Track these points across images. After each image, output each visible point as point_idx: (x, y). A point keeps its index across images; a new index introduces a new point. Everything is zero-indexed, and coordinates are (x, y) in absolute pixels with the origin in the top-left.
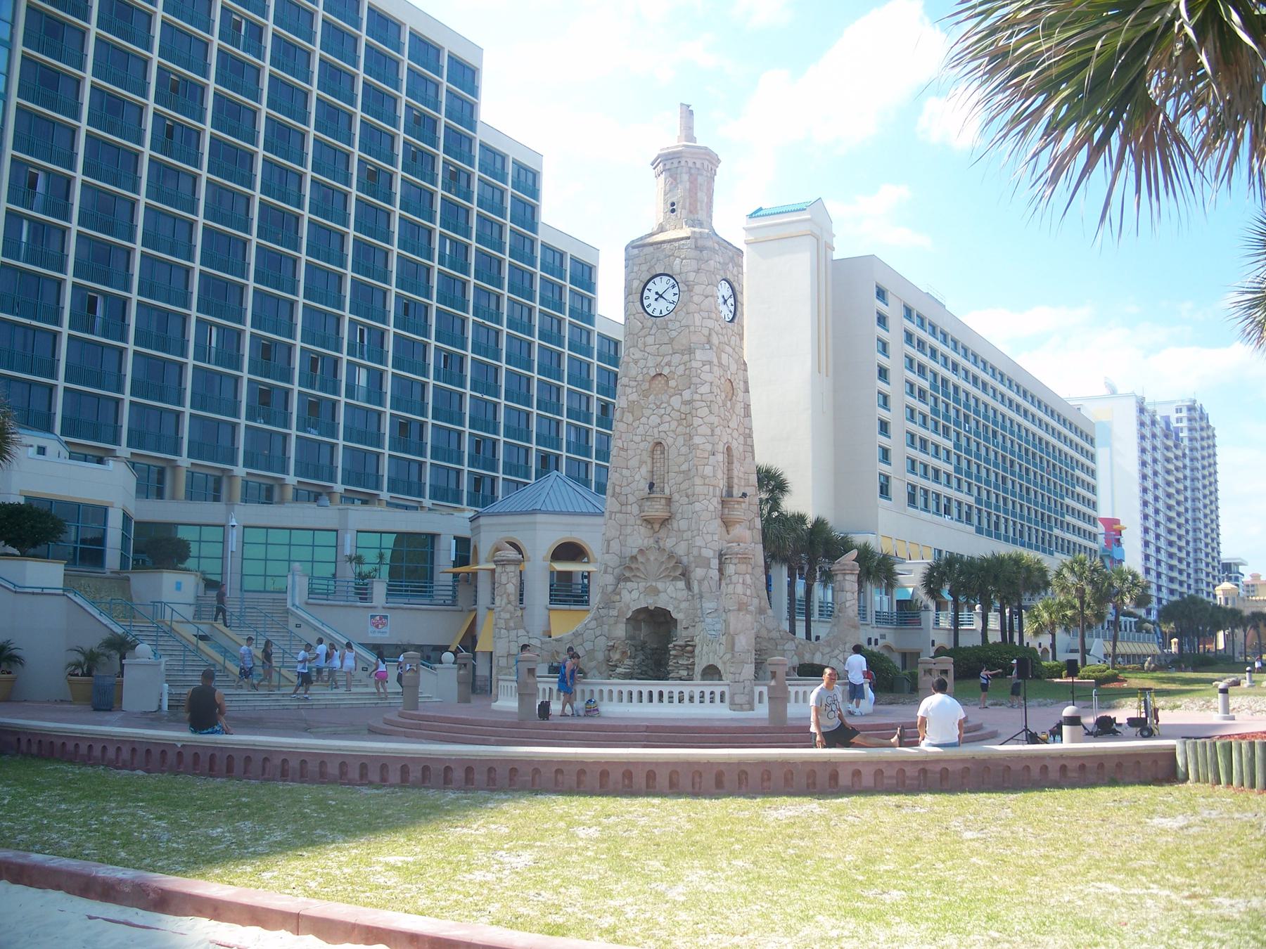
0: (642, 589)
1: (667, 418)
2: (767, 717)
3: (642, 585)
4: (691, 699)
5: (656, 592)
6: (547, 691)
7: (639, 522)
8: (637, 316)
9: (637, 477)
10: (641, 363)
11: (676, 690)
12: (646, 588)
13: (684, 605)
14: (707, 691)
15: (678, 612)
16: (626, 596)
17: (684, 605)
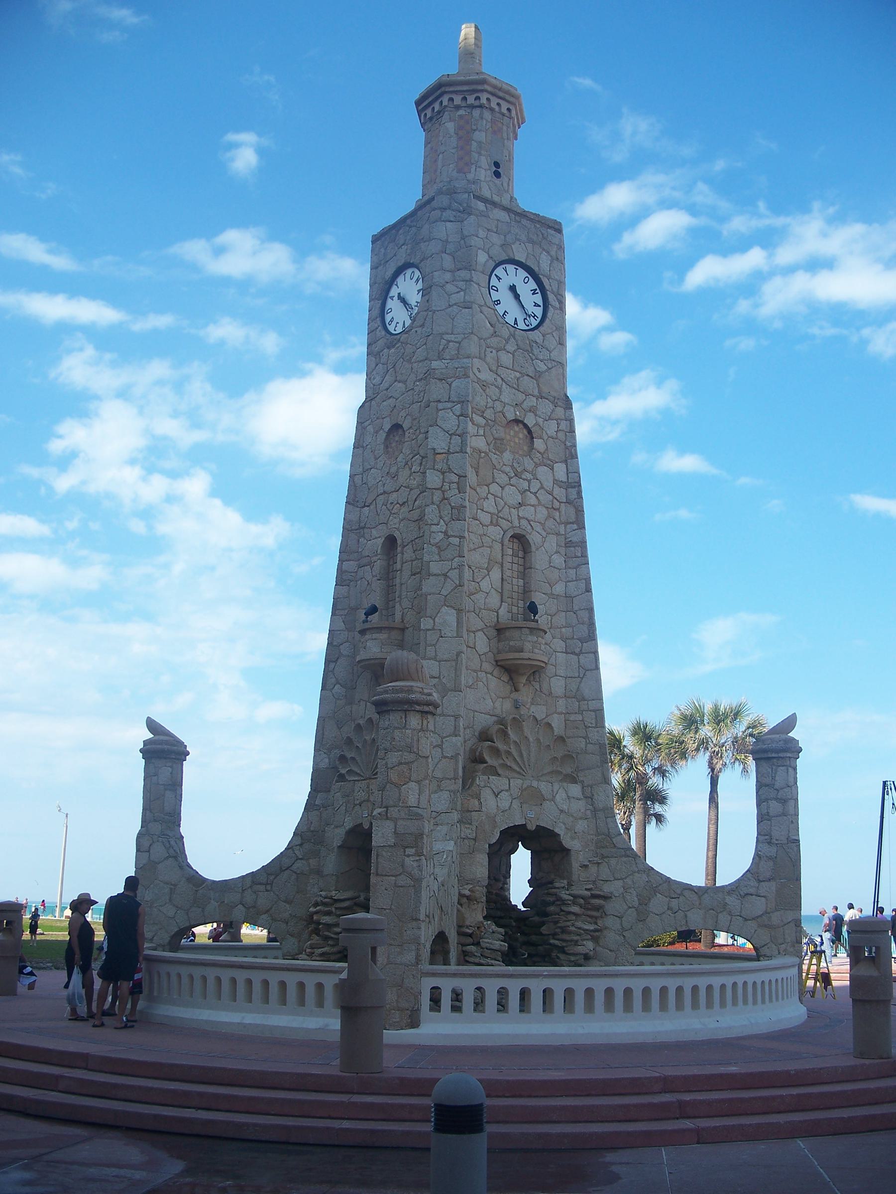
0: (516, 792)
1: (533, 500)
2: (337, 1037)
3: (516, 783)
4: (479, 1005)
5: (539, 799)
6: (702, 993)
7: (487, 666)
8: (485, 309)
9: (485, 585)
10: (493, 391)
11: (599, 986)
12: (522, 790)
13: (581, 826)
14: (514, 987)
15: (573, 838)
16: (490, 803)
17: (581, 826)
